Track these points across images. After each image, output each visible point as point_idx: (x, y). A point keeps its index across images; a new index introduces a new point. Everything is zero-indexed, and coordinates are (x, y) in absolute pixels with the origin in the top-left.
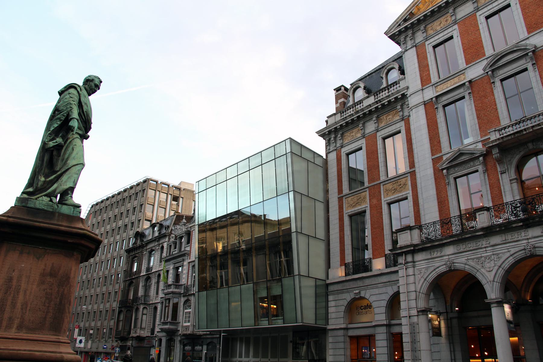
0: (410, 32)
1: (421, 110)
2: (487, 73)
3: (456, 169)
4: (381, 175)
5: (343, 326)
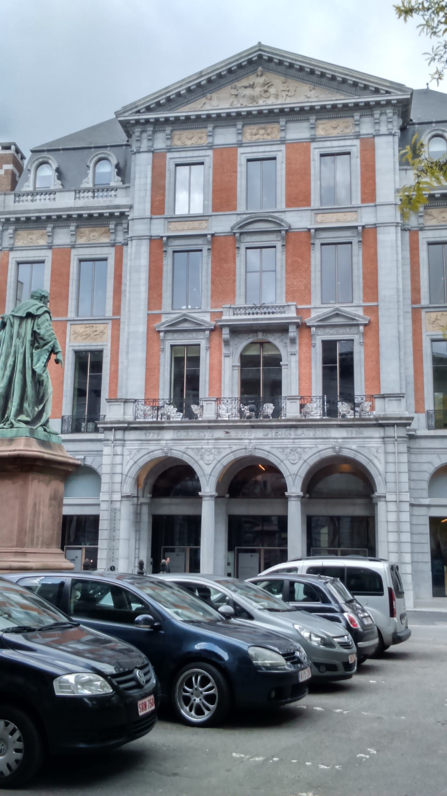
0: (150, 129)
1: (145, 247)
2: (235, 233)
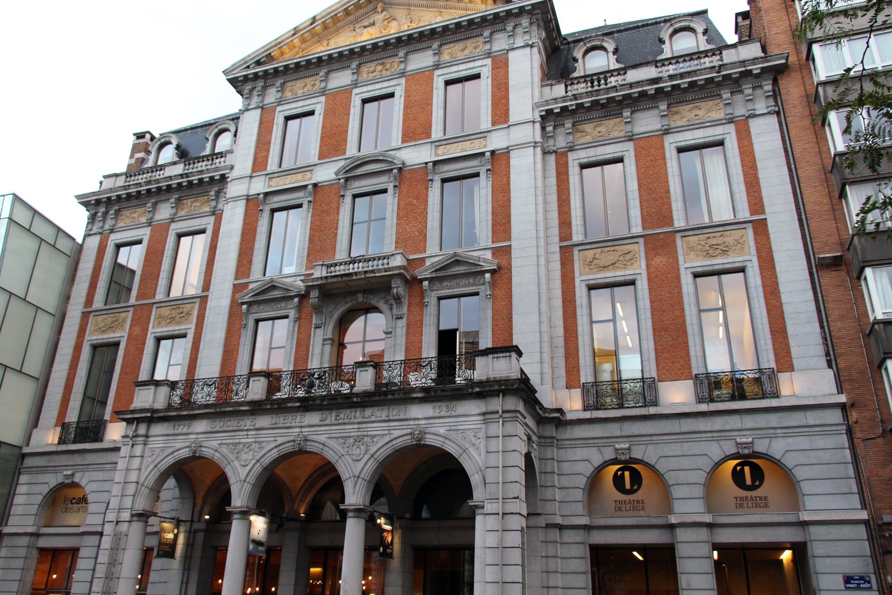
0: (260, 84)
2: (339, 179)
3: (262, 307)
4: (158, 291)
5: (30, 530)
